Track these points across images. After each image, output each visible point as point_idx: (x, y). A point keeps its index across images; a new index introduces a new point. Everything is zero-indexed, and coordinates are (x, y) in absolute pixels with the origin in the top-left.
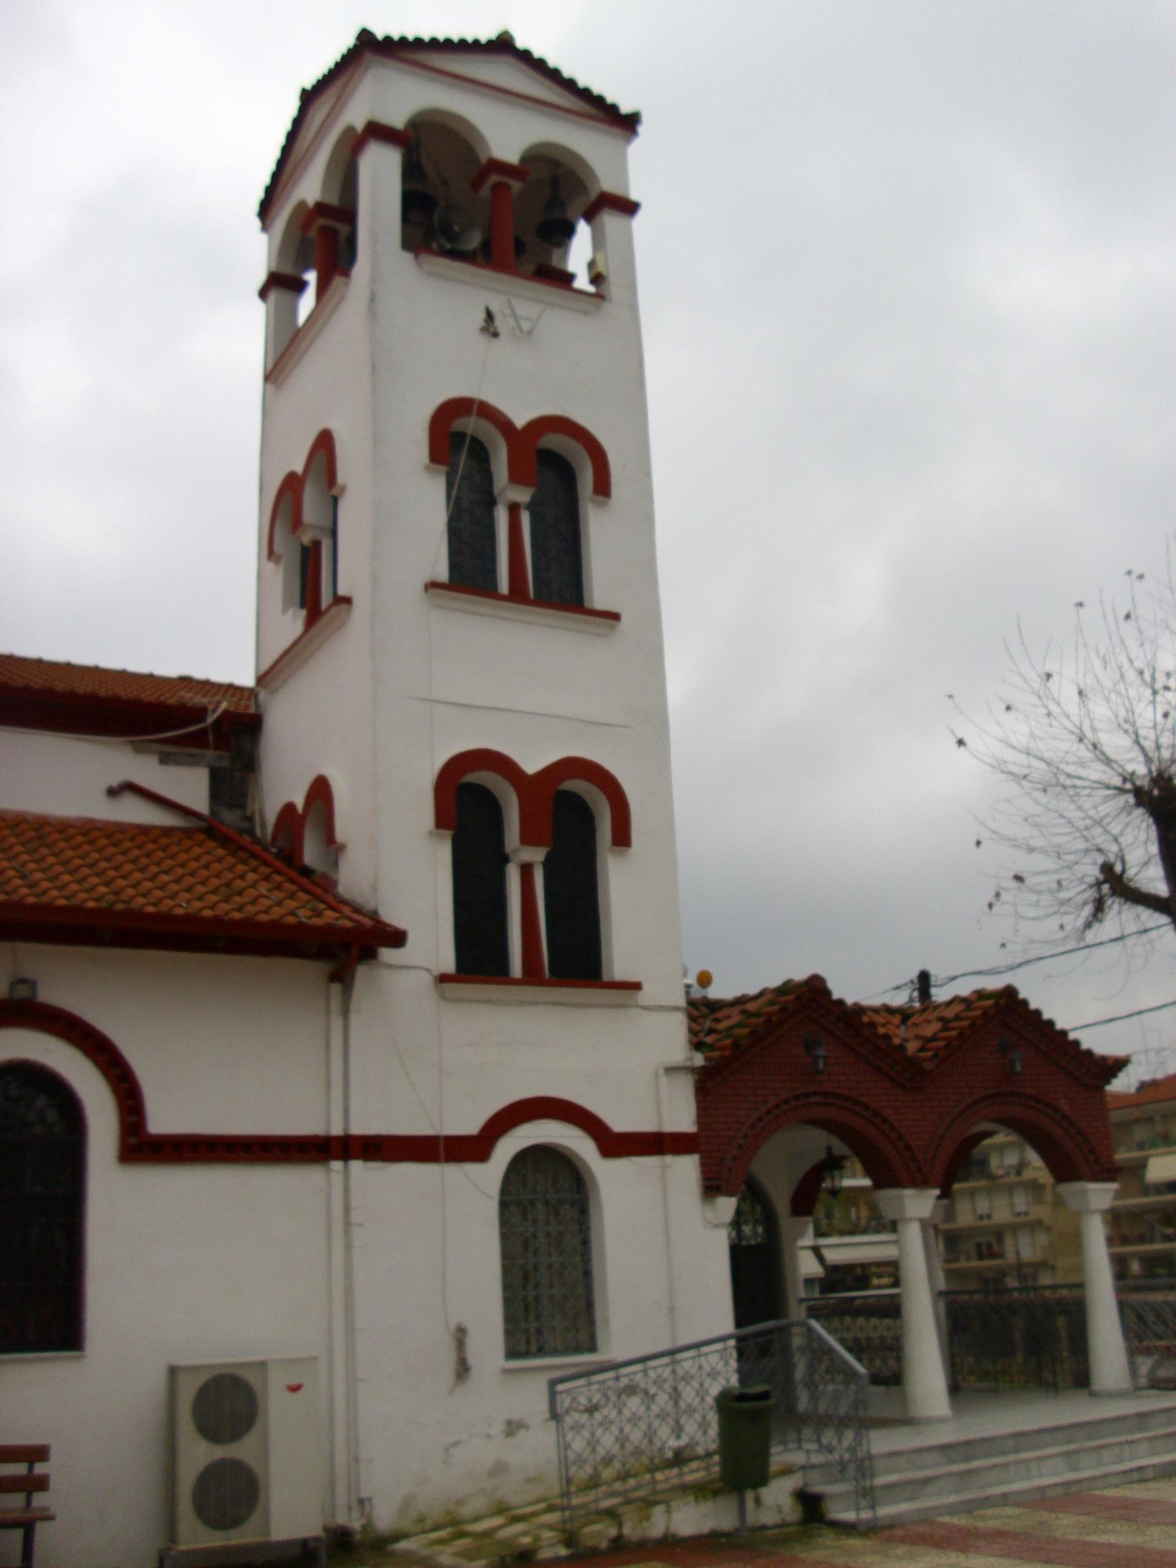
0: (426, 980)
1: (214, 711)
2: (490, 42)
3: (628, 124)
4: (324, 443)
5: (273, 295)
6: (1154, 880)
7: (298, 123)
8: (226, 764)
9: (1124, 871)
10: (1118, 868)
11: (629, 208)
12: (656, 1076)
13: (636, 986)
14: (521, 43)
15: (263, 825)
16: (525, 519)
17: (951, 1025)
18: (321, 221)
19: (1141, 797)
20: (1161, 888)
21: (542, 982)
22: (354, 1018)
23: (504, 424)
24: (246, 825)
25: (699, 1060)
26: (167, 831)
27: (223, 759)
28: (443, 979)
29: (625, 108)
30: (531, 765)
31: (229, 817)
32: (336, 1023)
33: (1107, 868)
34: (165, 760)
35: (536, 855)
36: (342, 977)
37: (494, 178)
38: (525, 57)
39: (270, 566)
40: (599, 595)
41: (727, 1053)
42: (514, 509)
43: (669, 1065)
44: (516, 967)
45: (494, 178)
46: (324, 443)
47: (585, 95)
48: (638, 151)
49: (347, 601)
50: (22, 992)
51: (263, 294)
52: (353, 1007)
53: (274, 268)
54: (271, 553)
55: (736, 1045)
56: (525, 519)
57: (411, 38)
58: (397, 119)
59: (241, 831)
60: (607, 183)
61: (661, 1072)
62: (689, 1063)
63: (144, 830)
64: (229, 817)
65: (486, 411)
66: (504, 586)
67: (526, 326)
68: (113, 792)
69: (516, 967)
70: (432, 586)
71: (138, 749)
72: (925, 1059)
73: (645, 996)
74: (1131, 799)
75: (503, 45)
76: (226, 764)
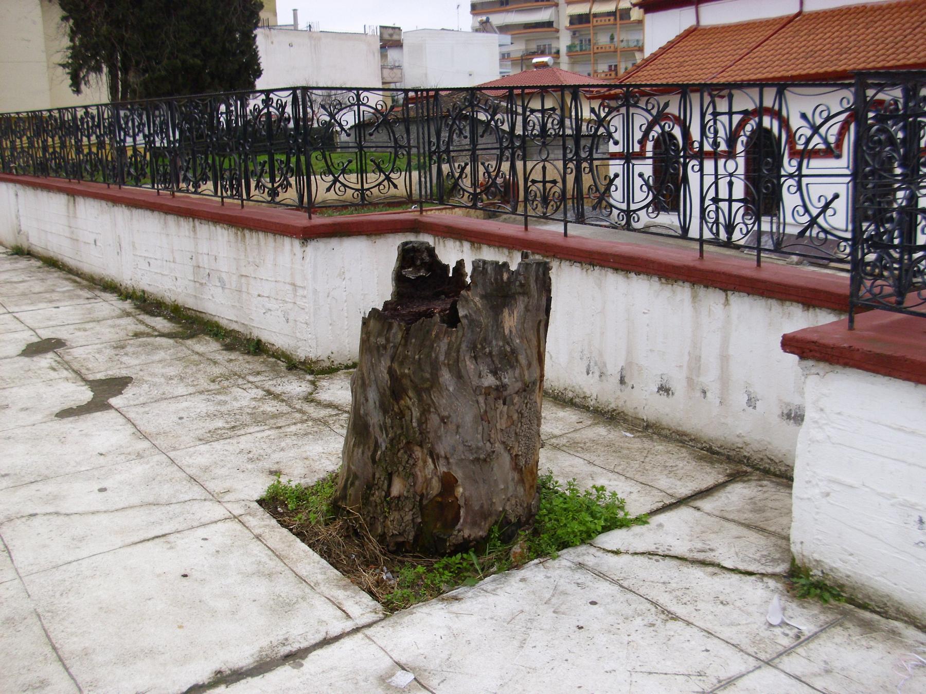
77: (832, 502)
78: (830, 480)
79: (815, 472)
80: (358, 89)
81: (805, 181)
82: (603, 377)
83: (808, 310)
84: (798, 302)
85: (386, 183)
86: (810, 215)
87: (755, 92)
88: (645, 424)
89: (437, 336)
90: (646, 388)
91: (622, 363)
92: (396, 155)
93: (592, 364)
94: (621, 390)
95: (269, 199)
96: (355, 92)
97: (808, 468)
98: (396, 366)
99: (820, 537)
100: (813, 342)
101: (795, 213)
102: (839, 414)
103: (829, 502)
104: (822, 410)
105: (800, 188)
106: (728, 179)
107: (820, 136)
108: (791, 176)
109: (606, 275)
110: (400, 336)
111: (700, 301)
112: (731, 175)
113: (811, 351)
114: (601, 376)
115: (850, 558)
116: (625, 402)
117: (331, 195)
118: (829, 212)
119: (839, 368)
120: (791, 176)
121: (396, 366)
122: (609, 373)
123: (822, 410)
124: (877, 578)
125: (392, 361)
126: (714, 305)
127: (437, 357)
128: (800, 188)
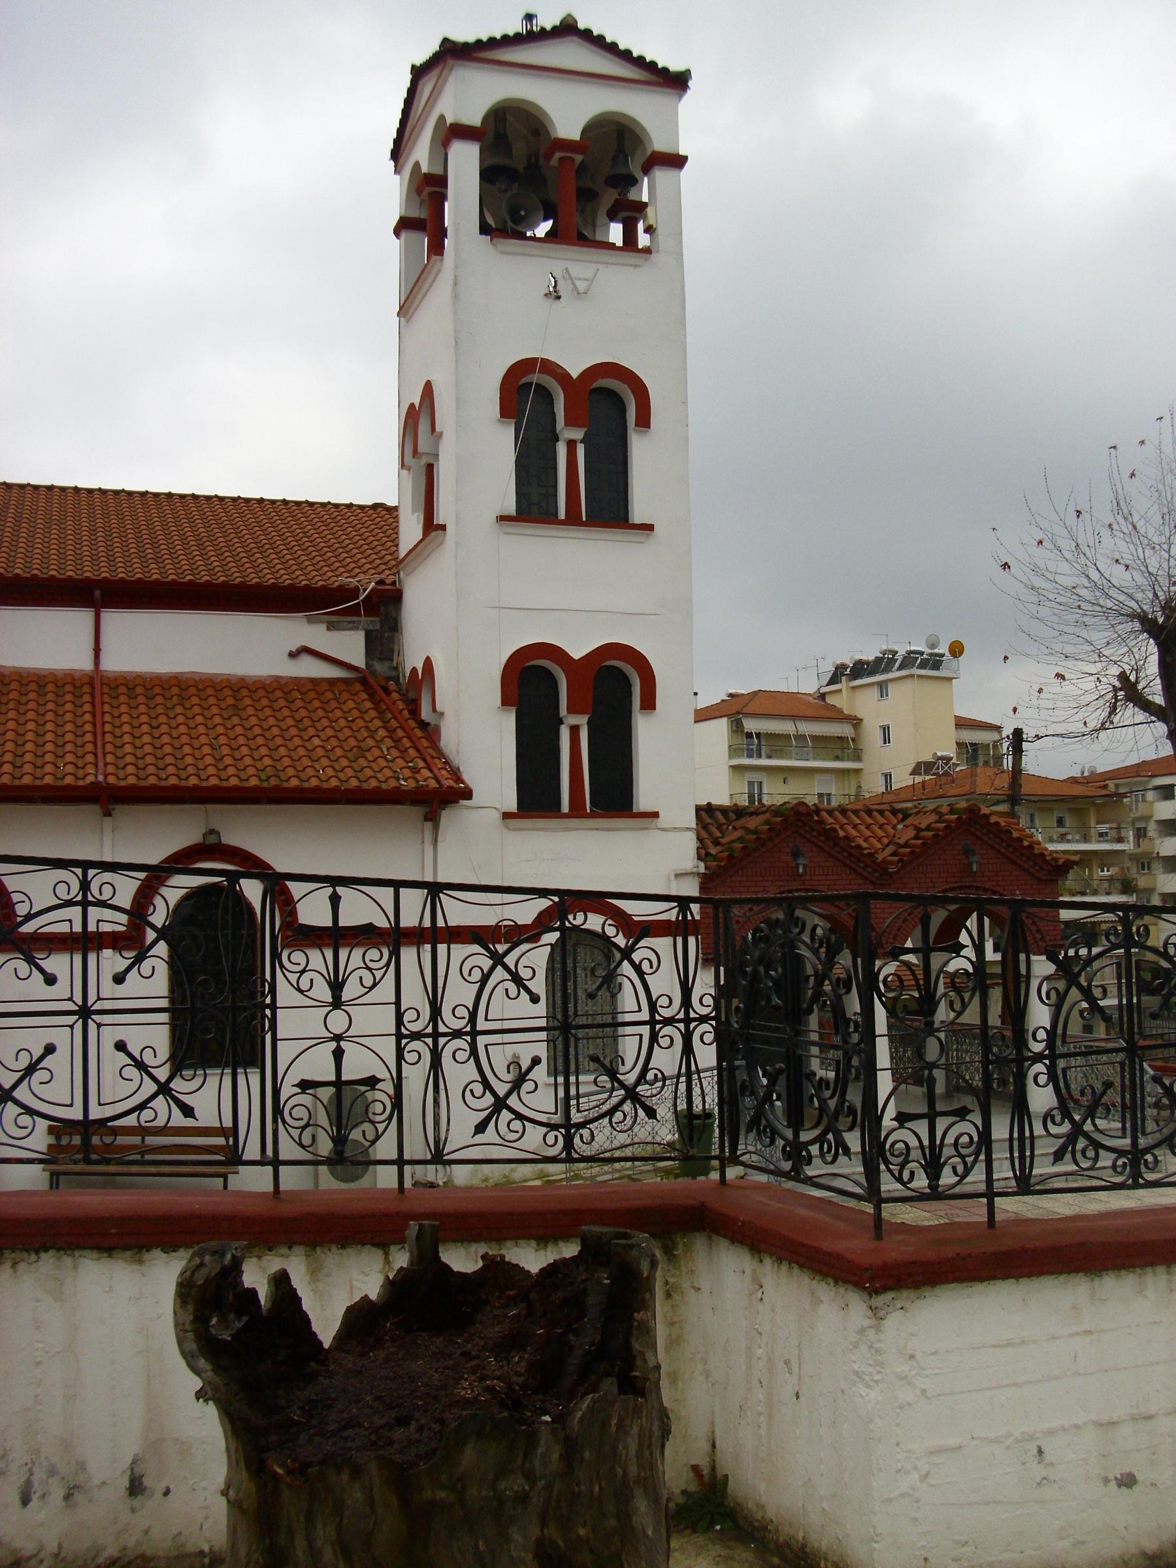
0: (497, 816)
1: (365, 590)
2: (555, 28)
3: (677, 82)
4: (428, 389)
5: (403, 235)
6: (1157, 695)
7: (412, 92)
8: (377, 627)
9: (1137, 682)
10: (1132, 678)
11: (677, 161)
12: (669, 879)
13: (656, 815)
14: (581, 25)
15: (404, 676)
16: (581, 450)
17: (922, 834)
18: (428, 190)
19: (1149, 626)
20: (1159, 700)
21: (585, 816)
22: (440, 845)
23: (561, 376)
24: (394, 673)
25: (702, 869)
26: (332, 682)
27: (374, 623)
28: (507, 816)
29: (675, 66)
30: (577, 653)
31: (380, 668)
32: (429, 849)
33: (1123, 677)
34: (331, 627)
35: (582, 720)
36: (433, 818)
37: (558, 155)
38: (587, 35)
39: (405, 472)
40: (638, 514)
41: (722, 864)
42: (571, 445)
43: (678, 872)
44: (565, 807)
45: (558, 155)
46: (428, 389)
47: (640, 62)
48: (689, 104)
49: (443, 528)
50: (212, 839)
51: (397, 232)
52: (439, 839)
53: (403, 213)
54: (403, 465)
55: (730, 857)
56: (581, 450)
57: (485, 39)
58: (474, 117)
59: (389, 678)
60: (659, 144)
61: (672, 877)
62: (695, 870)
63: (314, 682)
64: (380, 668)
65: (548, 367)
66: (562, 515)
67: (582, 287)
68: (293, 655)
69: (565, 807)
70: (503, 518)
71: (310, 620)
72: (892, 863)
73: (662, 821)
74: (1137, 625)
75: (567, 29)
76: (377, 627)
77: (935, 1482)
78: (932, 1453)
79: (909, 1451)
80: (86, 865)
81: (481, 1040)
82: (78, 1497)
83: (546, 1247)
84: (528, 1237)
85: (627, 1107)
86: (153, 1097)
87: (385, 895)
88: (207, 1560)
89: (620, 1426)
90: (204, 1484)
91: (129, 1450)
92: (654, 1038)
93: (39, 1475)
94: (133, 1510)
95: (787, 1166)
96: (79, 871)
97: (898, 1449)
98: (552, 1532)
99: (923, 1543)
100: (912, 1263)
101: (468, 1093)
102: (936, 1353)
103: (933, 1486)
104: (912, 1357)
105: (474, 1052)
106: (334, 1045)
107: (506, 968)
108: (457, 1034)
109: (76, 1268)
110: (555, 1456)
111: (328, 1275)
112: (338, 1038)
113: (910, 1276)
114: (68, 1497)
115: (965, 1549)
116: (146, 1532)
117: (490, 1145)
118: (527, 1086)
119: (926, 1291)
120: (457, 1034)
121: (552, 1532)
122: (96, 1481)
123: (912, 1357)
124: (1000, 1558)
125: (543, 1522)
126: (361, 1277)
127: (625, 1474)
128: (474, 1052)
